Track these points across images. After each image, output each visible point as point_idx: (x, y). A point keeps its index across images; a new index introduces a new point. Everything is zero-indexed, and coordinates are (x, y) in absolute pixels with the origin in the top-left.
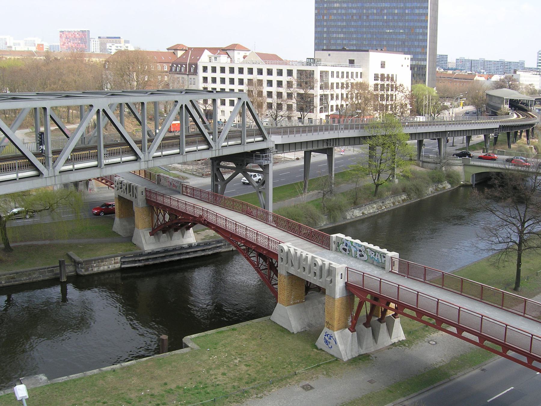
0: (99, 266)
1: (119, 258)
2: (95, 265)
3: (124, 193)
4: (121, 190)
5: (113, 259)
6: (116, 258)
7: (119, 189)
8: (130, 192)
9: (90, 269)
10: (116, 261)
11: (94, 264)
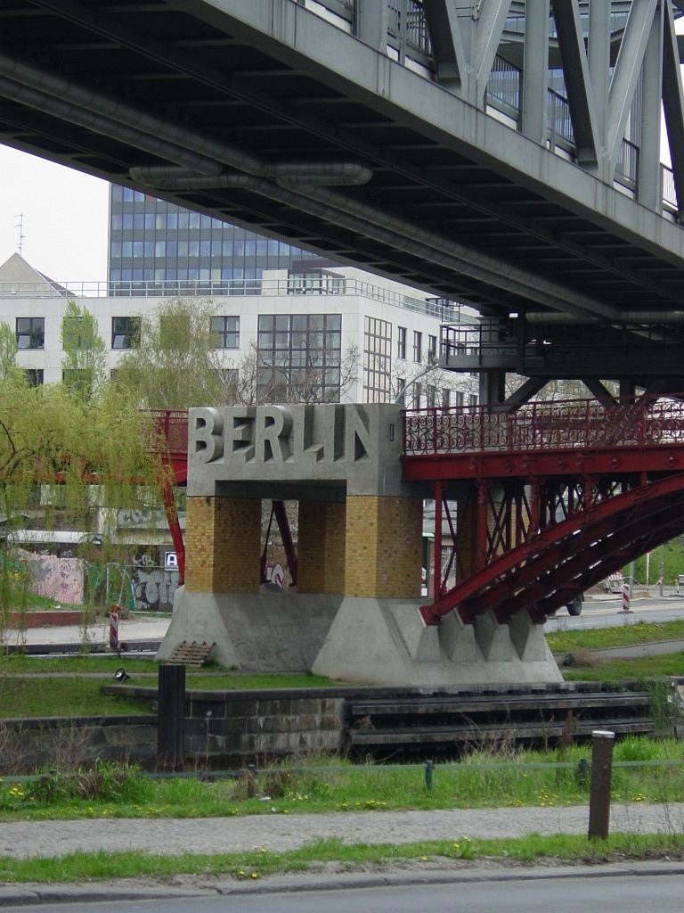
0: (272, 730)
1: (338, 703)
2: (261, 721)
3: (269, 454)
4: (245, 450)
5: (319, 701)
6: (329, 702)
7: (228, 446)
8: (309, 442)
9: (245, 737)
10: (327, 715)
11: (260, 714)
